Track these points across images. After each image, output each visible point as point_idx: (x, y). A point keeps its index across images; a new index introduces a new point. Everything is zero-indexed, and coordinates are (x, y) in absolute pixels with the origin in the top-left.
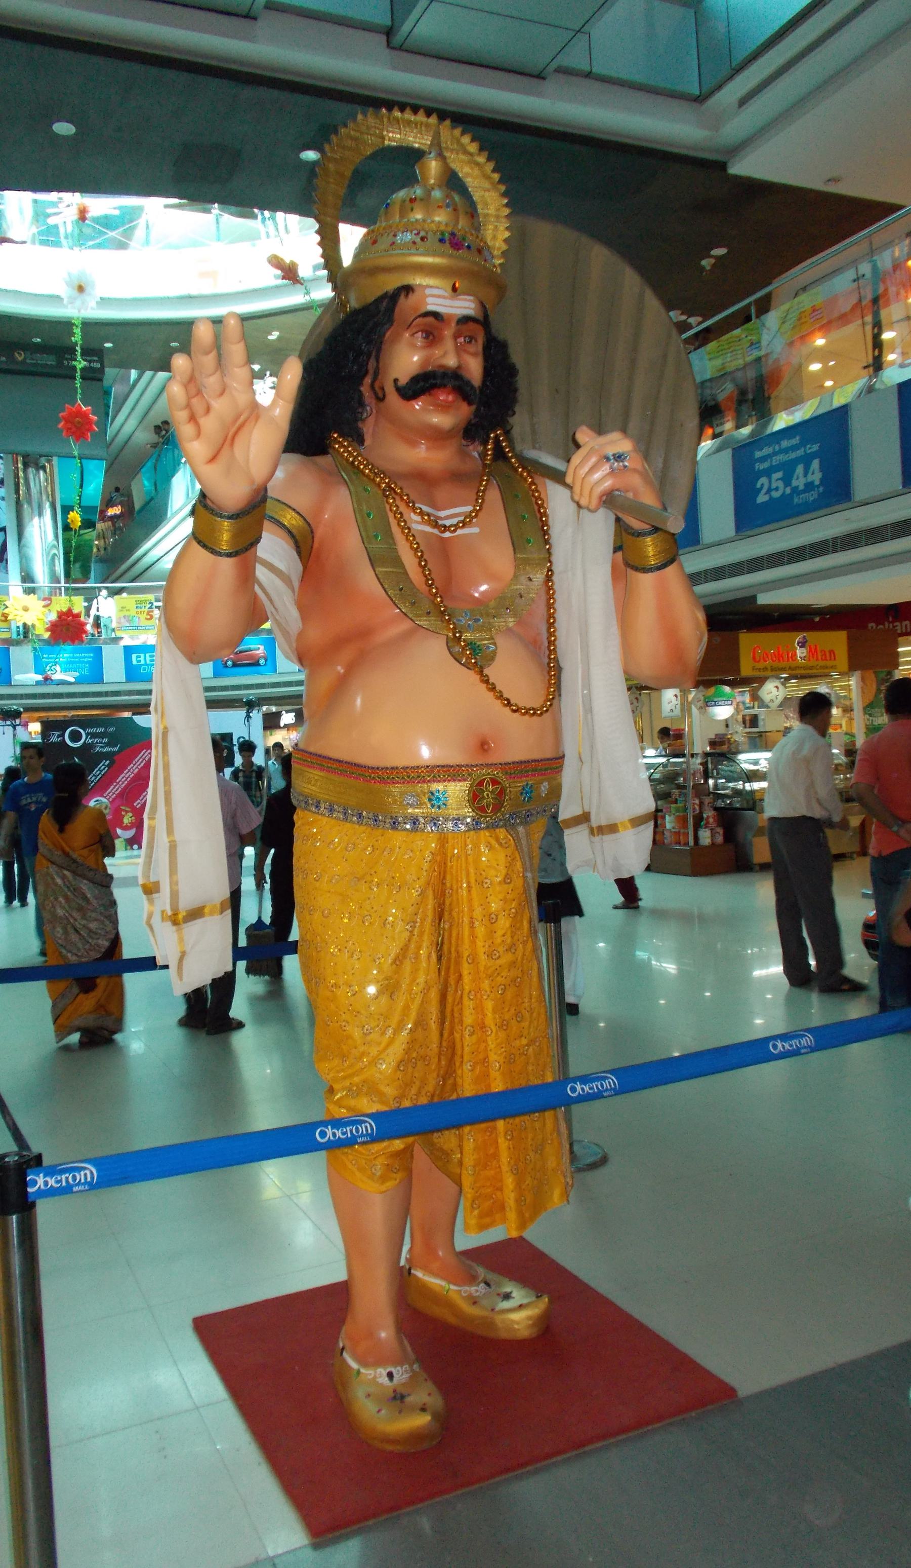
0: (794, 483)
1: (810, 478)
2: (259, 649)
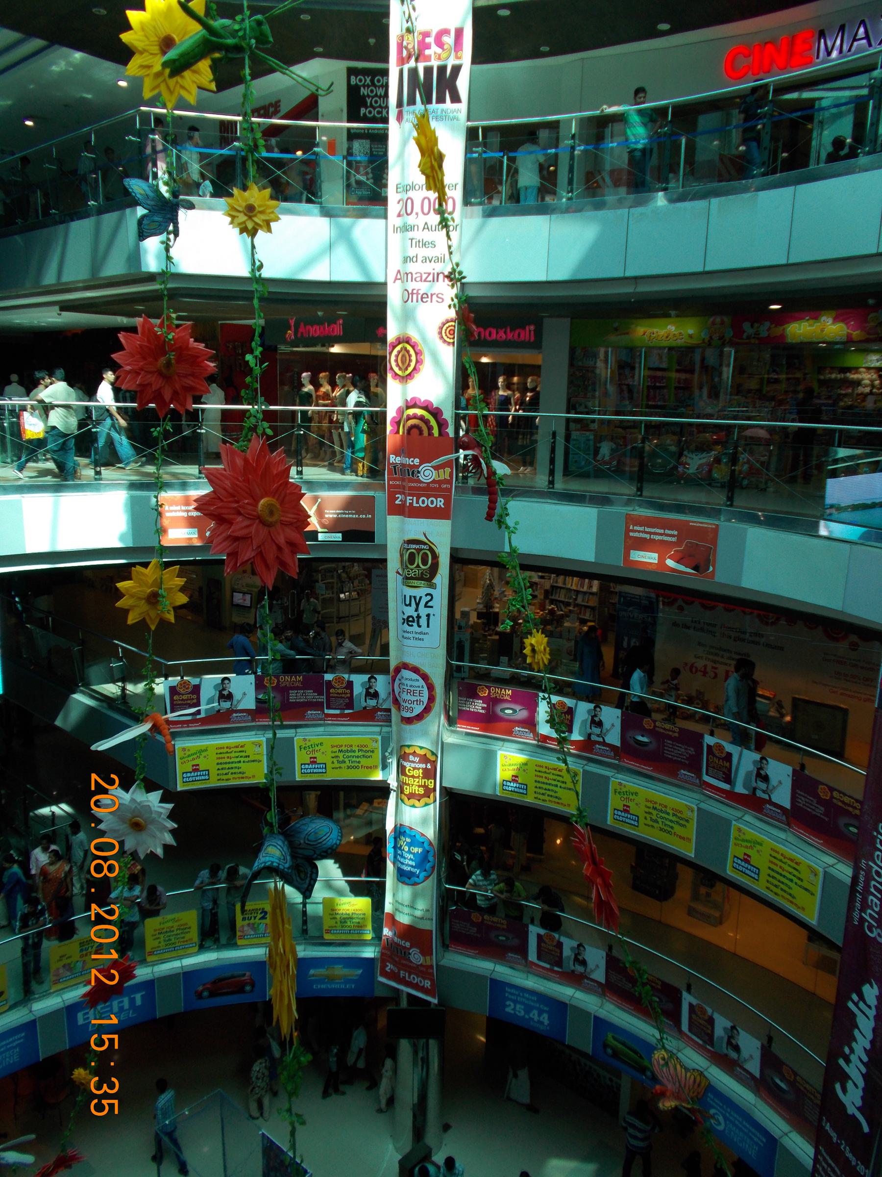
0: (531, 1015)
1: (541, 1019)
2: (244, 975)
